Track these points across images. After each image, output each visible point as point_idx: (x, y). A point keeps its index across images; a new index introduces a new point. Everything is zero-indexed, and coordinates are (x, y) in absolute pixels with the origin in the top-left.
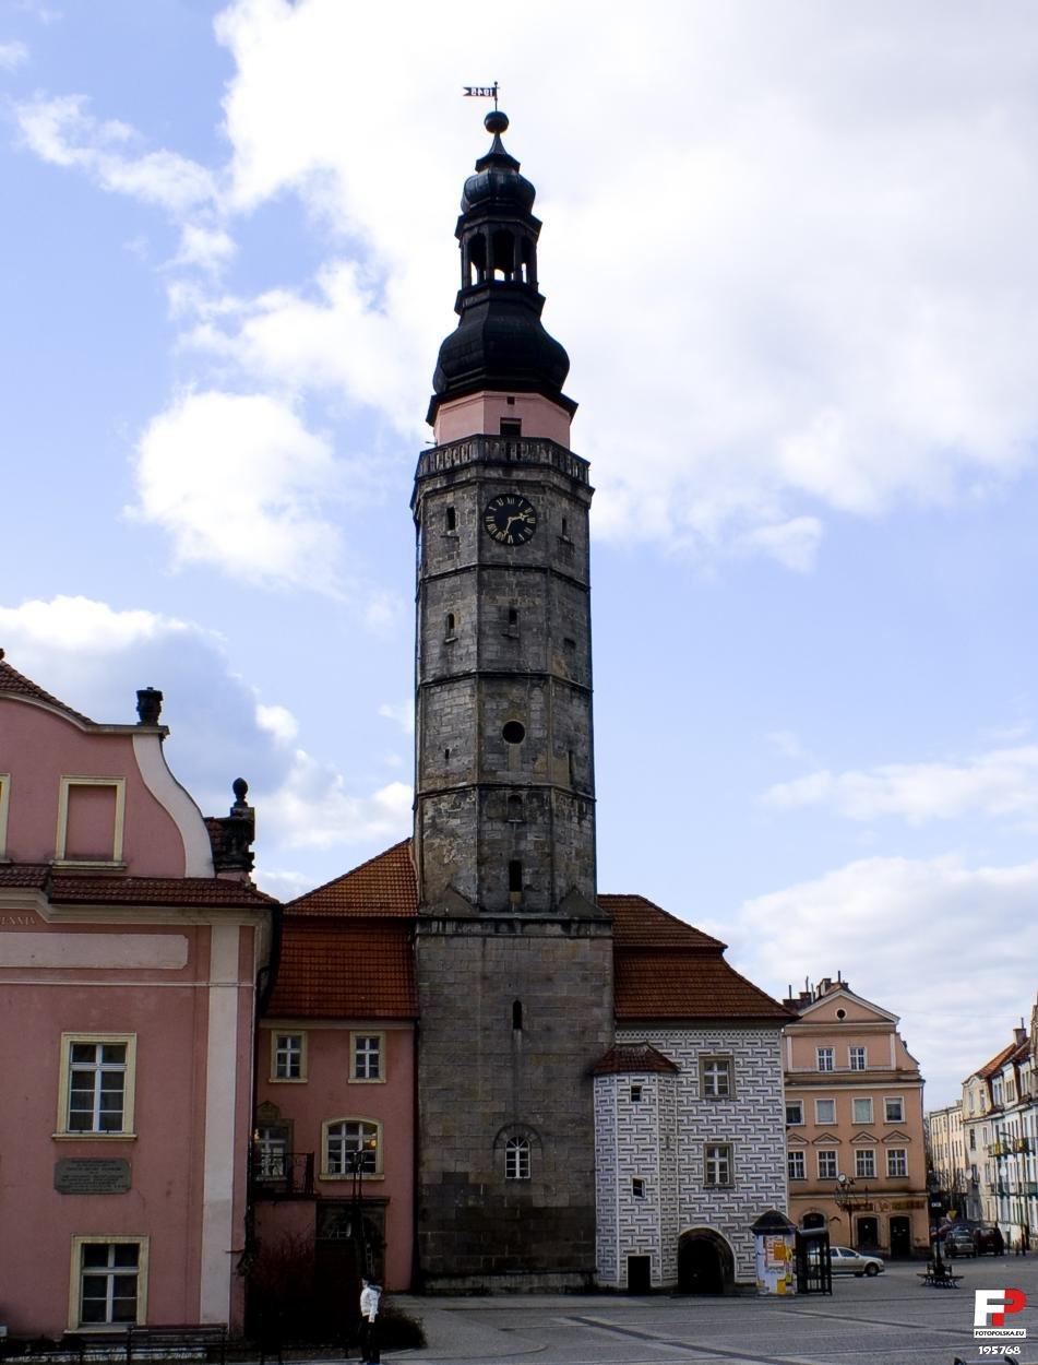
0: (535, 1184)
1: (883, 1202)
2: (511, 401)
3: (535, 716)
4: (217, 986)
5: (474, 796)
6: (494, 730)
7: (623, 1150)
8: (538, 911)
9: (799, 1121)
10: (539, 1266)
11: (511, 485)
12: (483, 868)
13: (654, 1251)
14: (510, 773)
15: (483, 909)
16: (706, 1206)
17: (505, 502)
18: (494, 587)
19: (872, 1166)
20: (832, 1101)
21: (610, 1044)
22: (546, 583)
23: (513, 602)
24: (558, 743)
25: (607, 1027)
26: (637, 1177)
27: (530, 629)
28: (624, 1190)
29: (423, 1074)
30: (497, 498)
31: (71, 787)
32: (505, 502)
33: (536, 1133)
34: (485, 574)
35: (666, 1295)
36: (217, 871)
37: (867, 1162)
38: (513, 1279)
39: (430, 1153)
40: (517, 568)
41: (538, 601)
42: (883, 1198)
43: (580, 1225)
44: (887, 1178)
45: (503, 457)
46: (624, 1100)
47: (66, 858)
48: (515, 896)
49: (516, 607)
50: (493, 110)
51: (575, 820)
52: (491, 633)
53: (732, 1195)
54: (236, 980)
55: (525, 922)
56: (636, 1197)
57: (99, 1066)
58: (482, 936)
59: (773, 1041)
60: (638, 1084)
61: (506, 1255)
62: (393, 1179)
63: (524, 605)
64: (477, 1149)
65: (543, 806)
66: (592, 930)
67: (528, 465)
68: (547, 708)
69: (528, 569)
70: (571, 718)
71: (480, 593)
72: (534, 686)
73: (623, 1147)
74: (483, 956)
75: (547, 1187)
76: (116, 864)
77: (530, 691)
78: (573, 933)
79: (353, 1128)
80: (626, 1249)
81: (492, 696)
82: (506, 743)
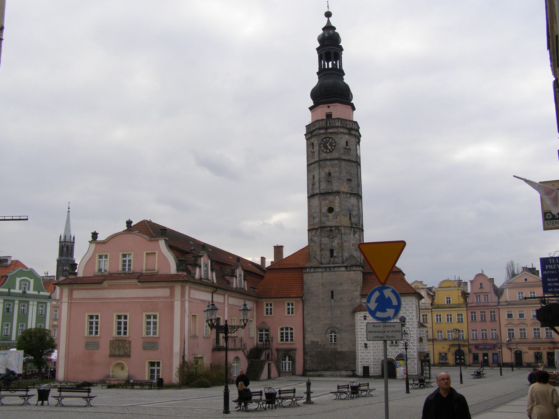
0: (338, 344)
1: (544, 347)
2: (329, 107)
3: (337, 204)
4: (176, 300)
5: (319, 231)
6: (325, 210)
7: (361, 334)
8: (338, 263)
9: (512, 318)
10: (340, 368)
11: (328, 134)
12: (322, 252)
13: (370, 365)
14: (330, 223)
15: (322, 264)
16: (390, 351)
17: (326, 139)
18: (323, 166)
19: (539, 333)
20: (524, 311)
21: (360, 303)
22: (339, 163)
23: (330, 170)
24: (344, 212)
25: (359, 297)
26: (366, 343)
27: (335, 178)
28: (361, 346)
29: (305, 313)
30: (324, 139)
31: (147, 253)
32: (326, 139)
33: (338, 329)
34: (321, 163)
35: (373, 378)
36: (178, 272)
37: (538, 332)
38: (332, 372)
39: (307, 336)
40: (330, 160)
41: (337, 169)
42: (544, 345)
43: (352, 356)
44: (545, 338)
45: (325, 126)
46: (361, 320)
47: (146, 271)
48: (332, 259)
49: (330, 172)
50: (327, 11)
51: (352, 235)
52: (323, 181)
53: (398, 348)
54: (180, 299)
55: (334, 267)
56: (365, 348)
57: (152, 320)
58: (321, 272)
59: (412, 300)
60: (365, 315)
61: (330, 365)
62: (298, 344)
63: (332, 171)
64: (321, 334)
65: (339, 232)
66: (354, 268)
67: (333, 127)
68: (340, 202)
69: (333, 159)
70: (350, 203)
71: (319, 169)
72: (336, 195)
73: (361, 334)
74: (322, 277)
75: (341, 345)
76: (156, 272)
77: (335, 197)
78: (349, 270)
79: (287, 329)
80: (362, 364)
81: (324, 200)
82: (328, 214)
